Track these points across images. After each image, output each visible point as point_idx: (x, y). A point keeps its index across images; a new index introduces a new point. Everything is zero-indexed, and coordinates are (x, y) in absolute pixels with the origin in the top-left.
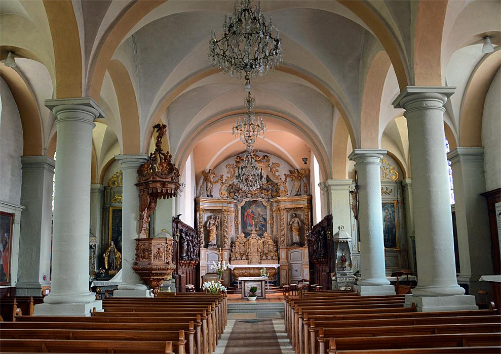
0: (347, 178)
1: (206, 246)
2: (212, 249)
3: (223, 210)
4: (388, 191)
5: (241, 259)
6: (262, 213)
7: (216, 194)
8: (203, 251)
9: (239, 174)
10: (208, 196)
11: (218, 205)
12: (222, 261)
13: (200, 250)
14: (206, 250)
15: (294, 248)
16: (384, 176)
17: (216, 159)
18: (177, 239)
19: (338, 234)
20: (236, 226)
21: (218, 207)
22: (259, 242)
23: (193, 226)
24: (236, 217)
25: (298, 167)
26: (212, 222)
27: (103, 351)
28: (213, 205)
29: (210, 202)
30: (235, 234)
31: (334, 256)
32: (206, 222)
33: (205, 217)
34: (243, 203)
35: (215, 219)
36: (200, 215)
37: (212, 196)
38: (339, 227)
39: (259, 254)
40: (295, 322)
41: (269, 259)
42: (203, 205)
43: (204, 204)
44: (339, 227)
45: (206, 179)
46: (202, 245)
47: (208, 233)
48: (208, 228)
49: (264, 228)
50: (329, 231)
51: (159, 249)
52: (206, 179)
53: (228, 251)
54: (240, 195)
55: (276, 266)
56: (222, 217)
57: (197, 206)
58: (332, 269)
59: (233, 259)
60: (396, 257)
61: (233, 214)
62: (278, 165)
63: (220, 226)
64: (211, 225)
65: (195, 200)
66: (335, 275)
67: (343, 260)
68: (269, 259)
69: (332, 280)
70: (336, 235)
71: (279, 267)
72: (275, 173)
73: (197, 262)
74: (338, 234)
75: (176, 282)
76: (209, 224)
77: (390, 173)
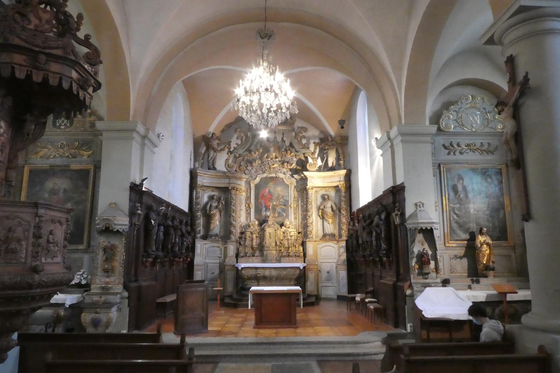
0: (427, 123)
2: (213, 241)
3: (230, 188)
4: (491, 149)
5: (253, 256)
6: (281, 194)
7: (220, 165)
8: (201, 246)
10: (209, 169)
14: (205, 242)
15: (326, 241)
16: (486, 124)
17: (220, 123)
18: (138, 221)
19: (414, 215)
20: (247, 211)
21: (223, 183)
22: (278, 232)
23: (186, 209)
24: (248, 198)
25: (332, 133)
26: (215, 204)
27: (463, 135)
28: (216, 181)
30: (245, 221)
31: (407, 251)
32: (207, 204)
33: (205, 198)
34: (258, 180)
35: (219, 200)
37: (215, 169)
38: (416, 204)
39: (278, 249)
41: (291, 256)
42: (204, 179)
43: (203, 179)
44: (416, 204)
45: (209, 147)
46: (198, 236)
47: (208, 218)
48: (208, 212)
49: (284, 214)
50: (399, 210)
51: (10, 230)
52: (209, 147)
53: (235, 244)
54: (254, 169)
55: (301, 265)
56: (228, 197)
58: (402, 275)
59: (241, 255)
60: (508, 257)
61: (244, 194)
62: (305, 129)
63: (227, 209)
64: (213, 208)
66: (410, 286)
67: (423, 260)
68: (291, 256)
69: (406, 296)
70: (411, 216)
71: (304, 268)
72: (301, 140)
73: (189, 259)
74: (414, 215)
75: (128, 298)
76: (211, 206)
77: (495, 119)
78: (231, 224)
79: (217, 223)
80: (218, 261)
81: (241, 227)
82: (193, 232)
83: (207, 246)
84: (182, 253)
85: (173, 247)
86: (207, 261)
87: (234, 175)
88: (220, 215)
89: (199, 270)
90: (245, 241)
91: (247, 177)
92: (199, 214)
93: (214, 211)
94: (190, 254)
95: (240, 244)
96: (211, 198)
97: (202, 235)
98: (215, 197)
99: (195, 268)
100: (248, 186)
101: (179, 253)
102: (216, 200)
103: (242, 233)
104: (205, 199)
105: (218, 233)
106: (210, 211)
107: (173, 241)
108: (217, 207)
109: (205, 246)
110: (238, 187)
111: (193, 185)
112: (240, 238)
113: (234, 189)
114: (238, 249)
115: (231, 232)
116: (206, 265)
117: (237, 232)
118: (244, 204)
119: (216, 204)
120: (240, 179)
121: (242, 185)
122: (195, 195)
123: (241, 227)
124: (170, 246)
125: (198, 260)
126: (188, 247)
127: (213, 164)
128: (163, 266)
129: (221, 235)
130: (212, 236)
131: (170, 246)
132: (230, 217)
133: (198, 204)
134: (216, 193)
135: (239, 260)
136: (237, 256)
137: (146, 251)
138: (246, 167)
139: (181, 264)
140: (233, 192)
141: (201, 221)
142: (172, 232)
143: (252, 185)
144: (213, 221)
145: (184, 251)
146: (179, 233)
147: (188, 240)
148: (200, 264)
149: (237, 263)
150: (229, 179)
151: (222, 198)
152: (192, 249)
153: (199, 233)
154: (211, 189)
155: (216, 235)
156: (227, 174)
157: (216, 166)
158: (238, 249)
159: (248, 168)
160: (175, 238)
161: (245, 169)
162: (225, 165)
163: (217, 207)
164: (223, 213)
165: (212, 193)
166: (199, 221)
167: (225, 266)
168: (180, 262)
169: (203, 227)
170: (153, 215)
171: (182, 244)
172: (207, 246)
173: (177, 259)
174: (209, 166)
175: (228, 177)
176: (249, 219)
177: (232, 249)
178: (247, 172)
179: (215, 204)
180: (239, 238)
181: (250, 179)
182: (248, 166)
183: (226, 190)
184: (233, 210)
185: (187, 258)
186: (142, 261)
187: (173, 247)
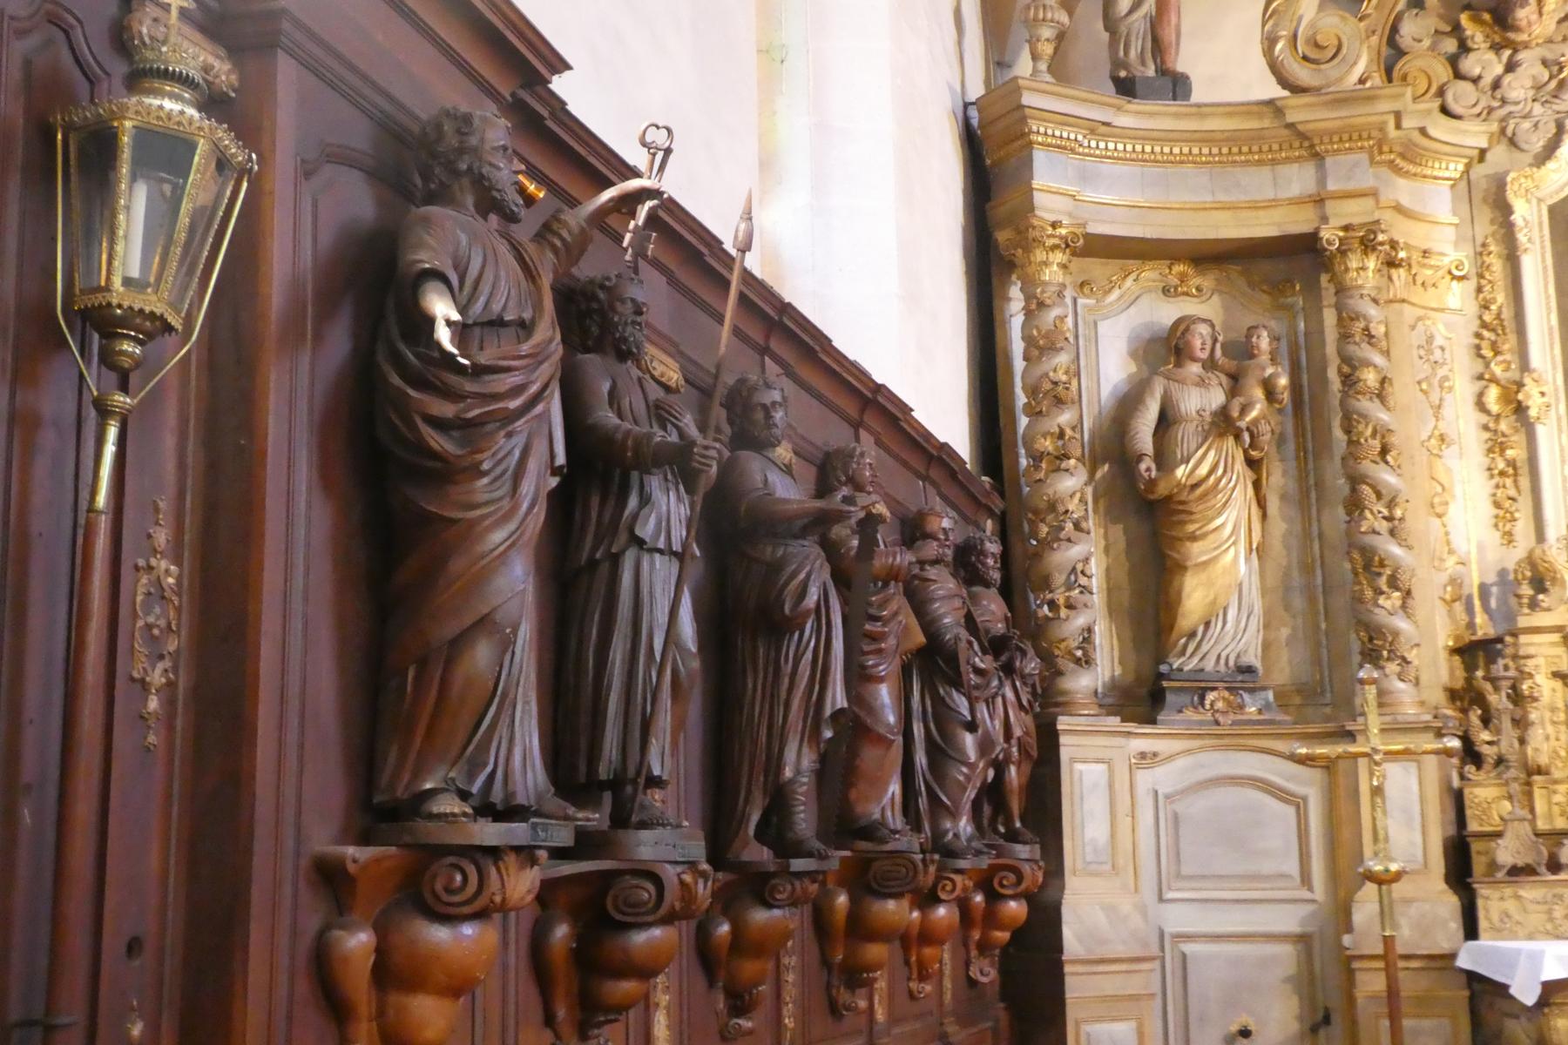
1: (1143, 698)
8: (1105, 776)
9: (1458, 75)
10: (1126, 87)
11: (1257, 183)
12: (1516, 475)
13: (1048, 739)
14: (1143, 740)
20: (1497, 445)
21: (1261, 205)
23: (947, 417)
26: (1200, 398)
29: (1155, 155)
30: (1495, 537)
32: (1129, 403)
35: (1235, 364)
36: (1034, 307)
37: (1176, 86)
40: (281, 726)
42: (1079, 184)
43: (1084, 178)
46: (1082, 683)
47: (1154, 524)
54: (1531, 66)
56: (1315, 334)
57: (1000, 208)
61: (1458, 296)
64: (1186, 435)
65: (973, 143)
76: (1166, 421)
78: (1370, 563)
79: (1230, 571)
80: (1288, 920)
81: (1457, 596)
82: (1027, 640)
83: (1163, 778)
84: (946, 851)
85: (839, 770)
86: (1178, 919)
87: (1360, 115)
88: (1261, 503)
89: (1116, 1006)
90: (1521, 723)
91: (1474, 135)
92: (1071, 485)
93: (1201, 462)
94: (1023, 851)
95: (1471, 754)
96: (1167, 349)
97: (1114, 686)
98: (1200, 338)
99: (1078, 987)
100: (1484, 226)
101: (909, 842)
102: (1210, 364)
103: (1475, 652)
104: (1110, 366)
105: (1253, 658)
106: (1164, 458)
107: (837, 697)
108: (1223, 424)
109: (1145, 779)
110: (1401, 230)
111: (992, 253)
112: (1466, 697)
113: (1368, 245)
114: (1458, 802)
115: (1377, 646)
116: (1167, 957)
117: (1427, 635)
118: (1463, 389)
119: (1217, 398)
120: (1409, 156)
121: (1433, 217)
122: (1016, 323)
123: (1457, 596)
124: (798, 762)
125: (1091, 914)
126: (993, 793)
127: (1158, 47)
128: (740, 1003)
129: (1283, 671)
130: (1199, 689)
131: (798, 762)
132: (1355, 505)
133: (1051, 396)
134: (1205, 308)
135: (1492, 902)
136: (1460, 864)
137: (380, 811)
138: (1453, 61)
139: (945, 957)
140: (1364, 272)
141: (1087, 557)
142: (810, 578)
143: (1528, 214)
144: (1197, 551)
145: (965, 826)
146: (901, 629)
147: (992, 718)
148: (1120, 951)
149: (1471, 930)
150: (1318, 157)
151: (1264, 342)
152: (1031, 805)
153: (1086, 662)
154: (1151, 273)
155: (1243, 676)
156: (1301, 112)
157: (1183, 63)
158: (1458, 802)
159: (1470, 65)
160: (858, 677)
161: (1442, 72)
162: (1270, 42)
163: (1223, 424)
164: (1277, 478)
165: (1167, 313)
166: (1073, 552)
167: (1347, 965)
168: (927, 936)
169: (1112, 610)
170: (445, 235)
171: (941, 753)
172: (1163, 778)
173: (895, 911)
174: (1117, 64)
175: (1309, 147)
176: (1523, 527)
177: (1404, 814)
178: (1462, 95)
179: (1200, 398)
180: (1453, 695)
181: (1499, 156)
182: (1464, 48)
183: (1292, 265)
184: (1382, 432)
185: (993, 897)
186: (323, 966)
187: (839, 770)
